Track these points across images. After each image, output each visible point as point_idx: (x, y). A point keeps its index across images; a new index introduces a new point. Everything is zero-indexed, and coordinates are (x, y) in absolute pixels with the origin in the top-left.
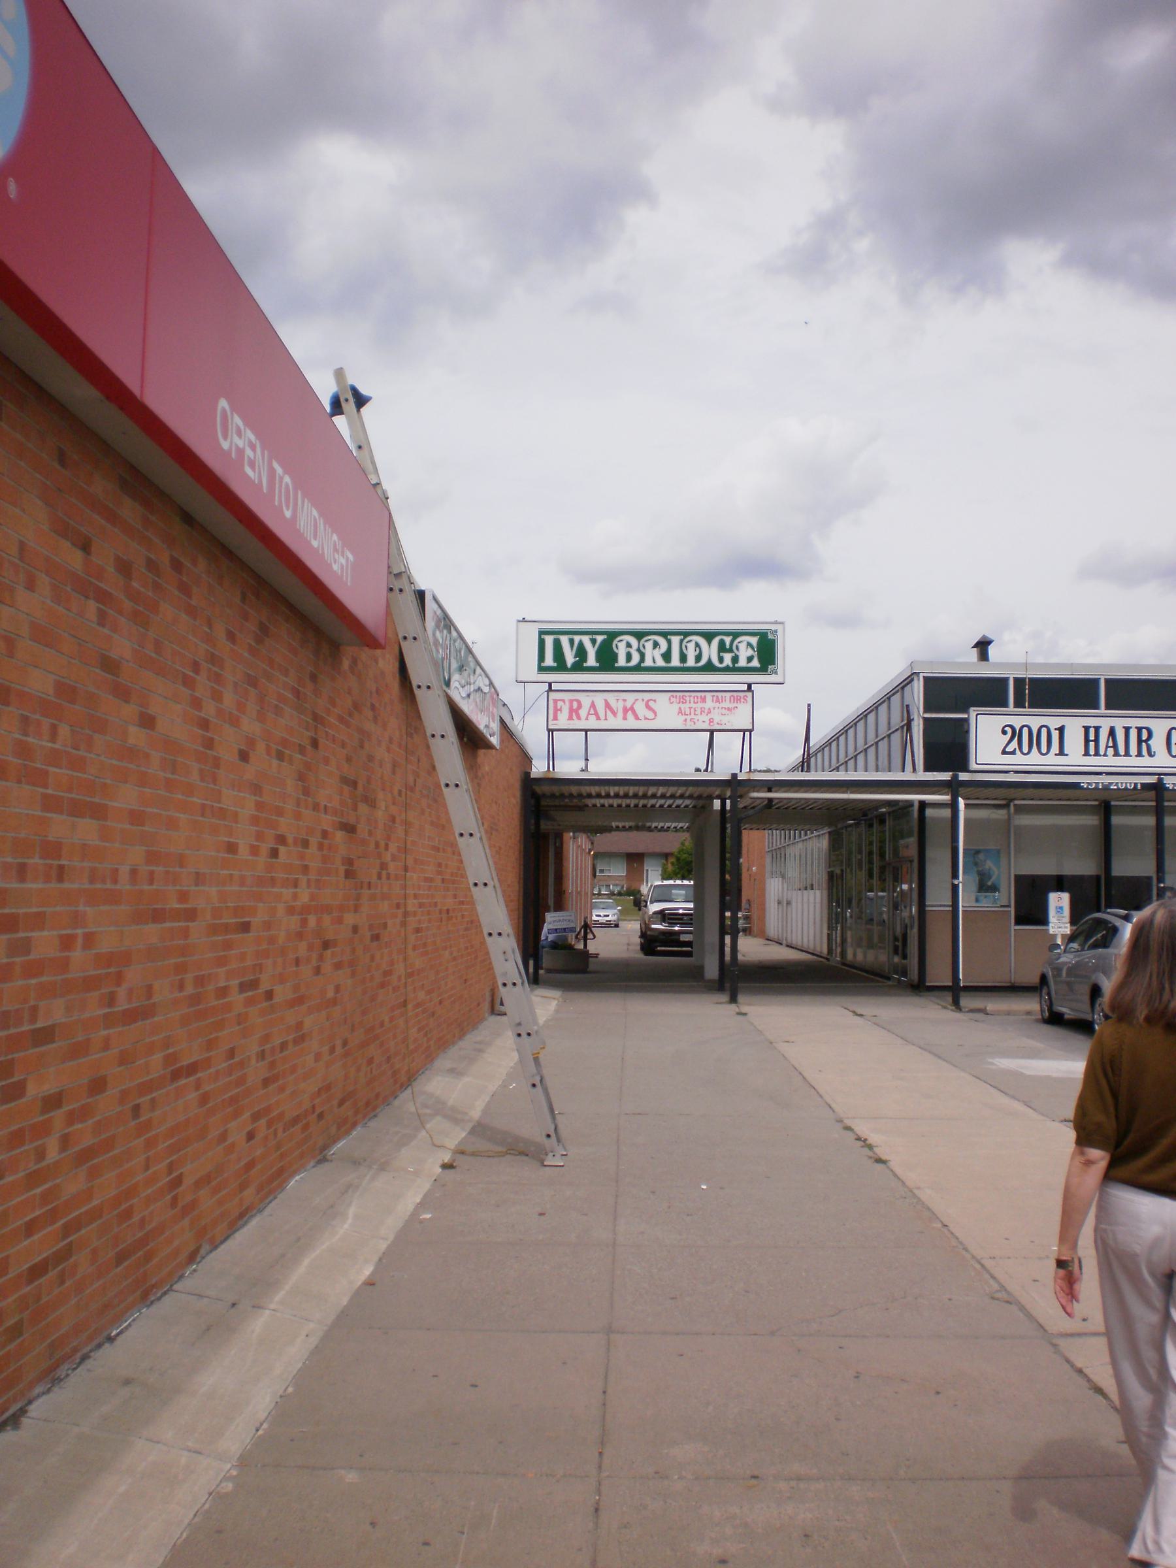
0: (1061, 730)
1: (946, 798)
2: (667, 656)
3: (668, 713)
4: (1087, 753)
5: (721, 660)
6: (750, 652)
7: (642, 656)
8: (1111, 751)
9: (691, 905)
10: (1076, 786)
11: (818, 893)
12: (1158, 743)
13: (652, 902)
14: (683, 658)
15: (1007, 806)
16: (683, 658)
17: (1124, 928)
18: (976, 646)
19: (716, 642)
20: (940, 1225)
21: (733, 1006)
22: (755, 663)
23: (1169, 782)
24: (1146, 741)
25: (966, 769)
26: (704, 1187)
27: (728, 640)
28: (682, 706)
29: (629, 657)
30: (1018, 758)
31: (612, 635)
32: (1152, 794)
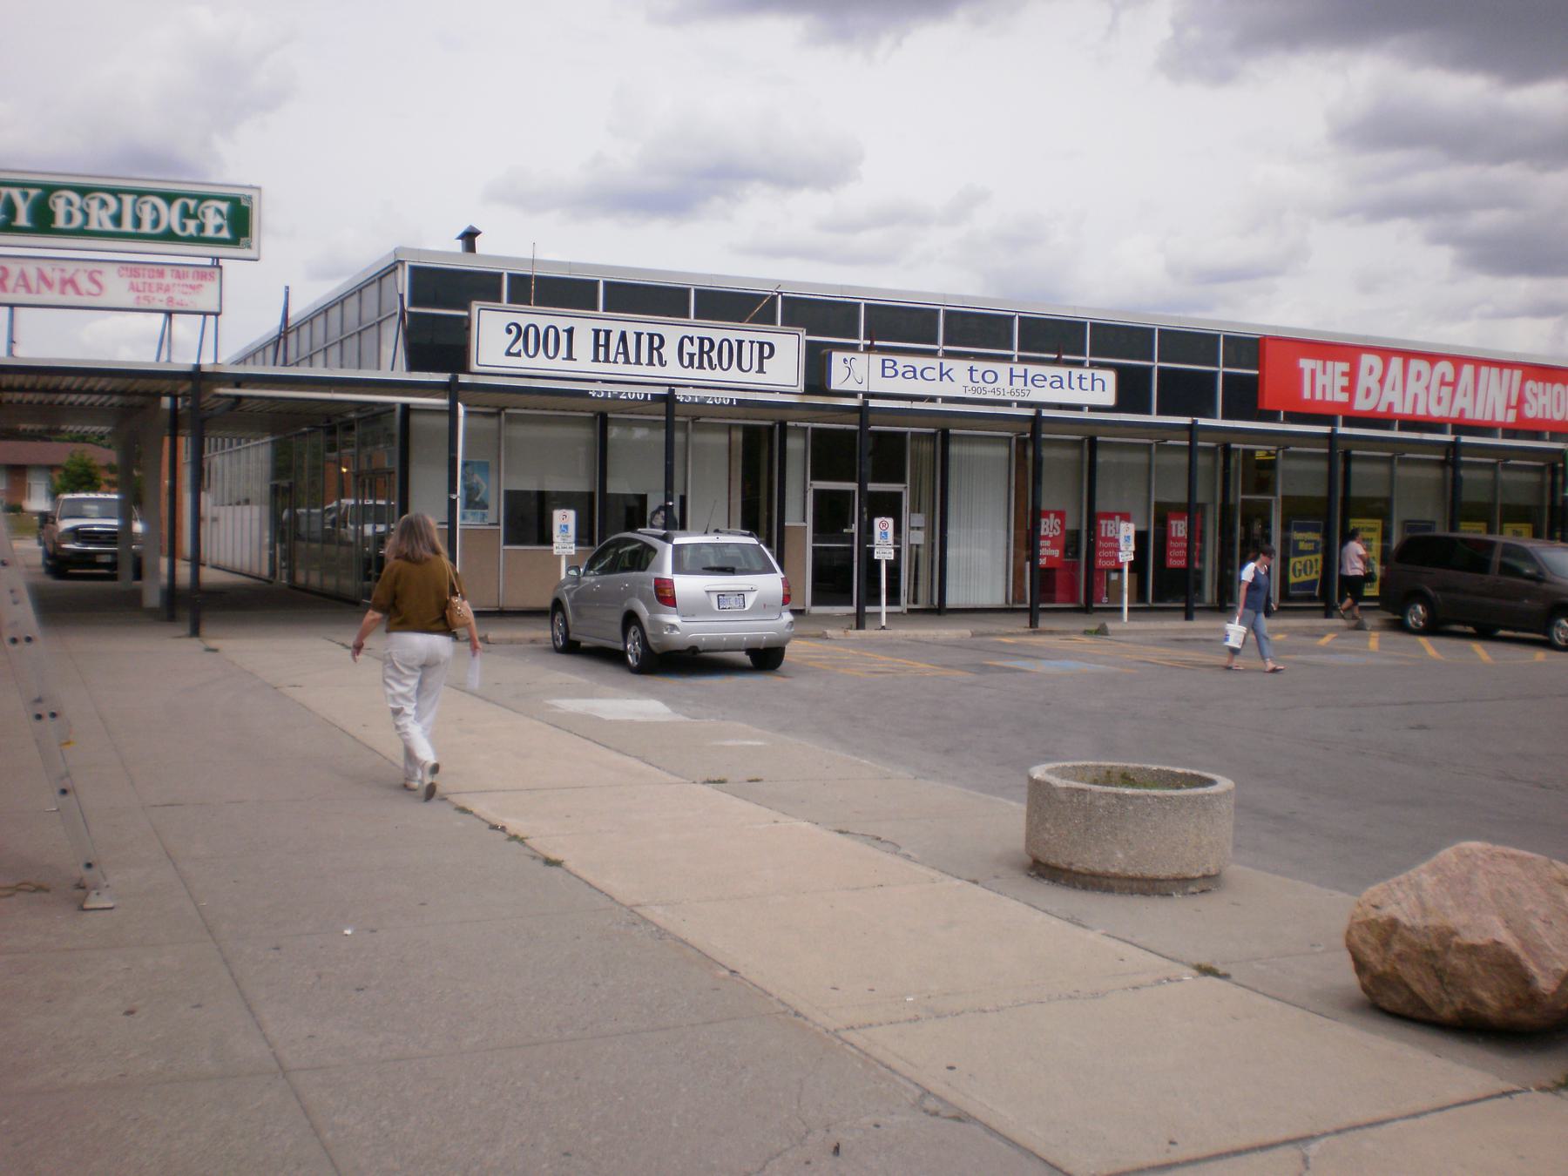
0: (570, 332)
1: (441, 402)
2: (117, 219)
3: (117, 288)
4: (596, 359)
5: (184, 227)
6: (219, 220)
7: (86, 215)
8: (621, 358)
9: (115, 522)
10: (585, 394)
11: (256, 509)
12: (670, 352)
13: (61, 518)
14: (138, 222)
15: (498, 414)
16: (138, 222)
17: (664, 549)
18: (462, 237)
19: (177, 205)
20: (726, 973)
21: (195, 641)
22: (225, 234)
23: (680, 393)
24: (658, 349)
25: (466, 370)
26: (348, 932)
27: (192, 203)
28: (135, 280)
29: (70, 217)
30: (524, 361)
31: (50, 189)
32: (662, 406)
